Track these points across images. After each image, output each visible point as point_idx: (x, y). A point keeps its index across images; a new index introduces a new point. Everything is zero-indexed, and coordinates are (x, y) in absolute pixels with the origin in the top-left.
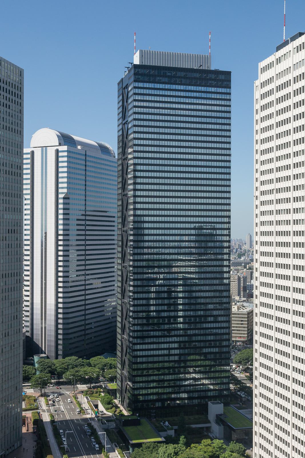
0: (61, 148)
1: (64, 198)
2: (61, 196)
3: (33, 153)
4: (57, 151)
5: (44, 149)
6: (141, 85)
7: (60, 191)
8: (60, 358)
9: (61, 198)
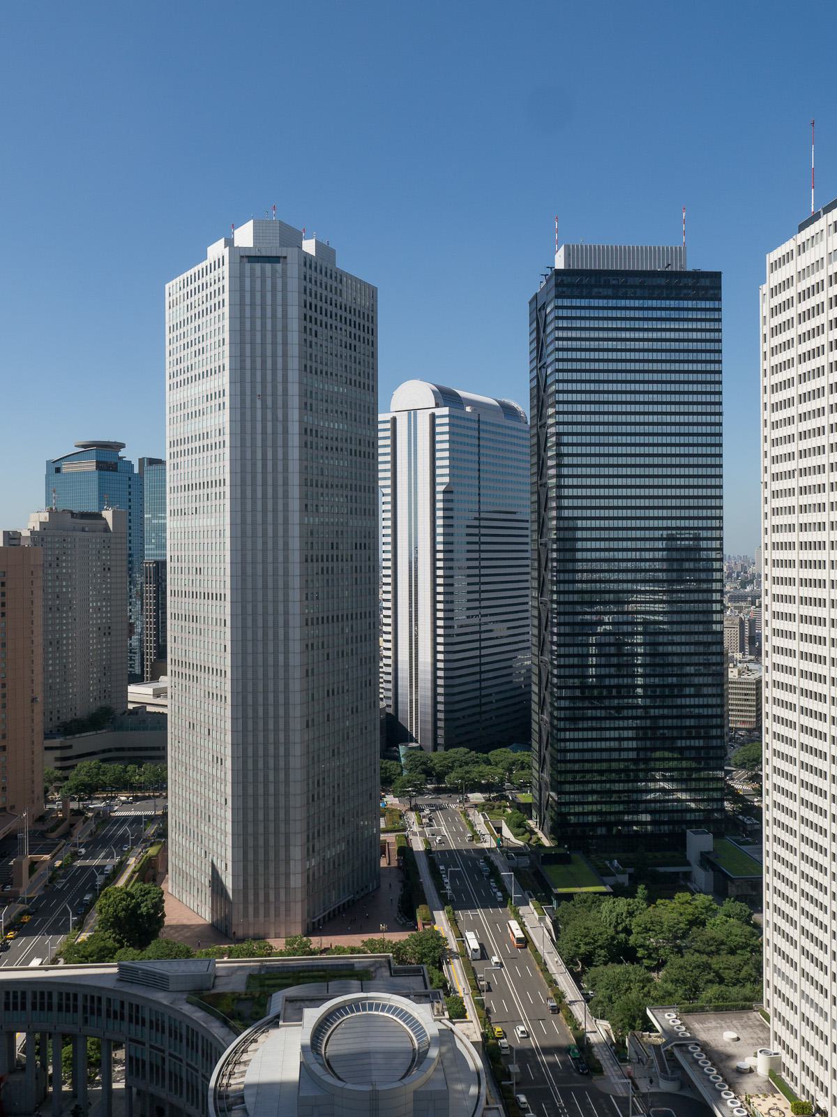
0: (438, 412)
1: (444, 492)
2: (440, 488)
3: (394, 420)
4: (433, 417)
5: (412, 413)
6: (567, 302)
7: (438, 480)
8: (441, 750)
9: (439, 492)
